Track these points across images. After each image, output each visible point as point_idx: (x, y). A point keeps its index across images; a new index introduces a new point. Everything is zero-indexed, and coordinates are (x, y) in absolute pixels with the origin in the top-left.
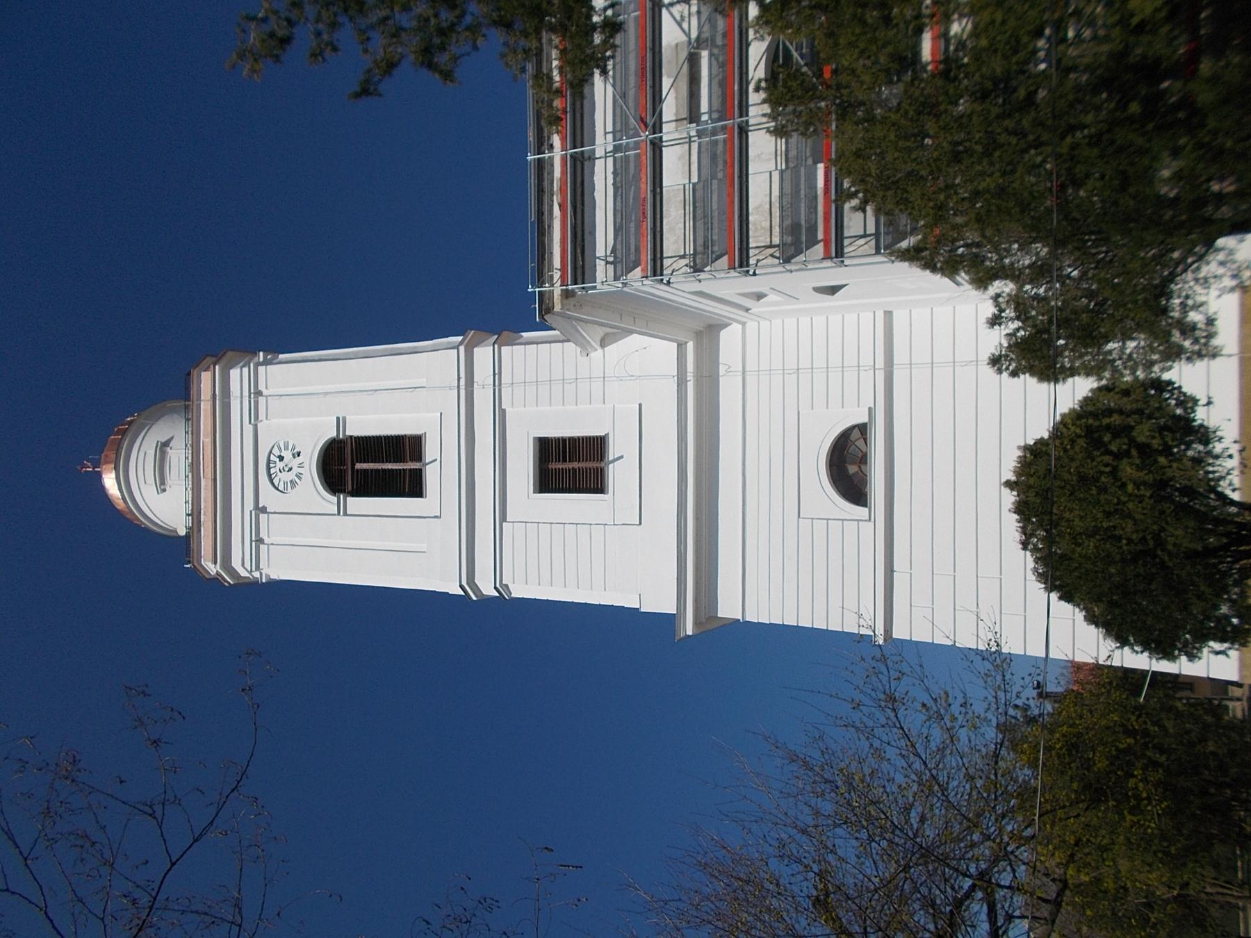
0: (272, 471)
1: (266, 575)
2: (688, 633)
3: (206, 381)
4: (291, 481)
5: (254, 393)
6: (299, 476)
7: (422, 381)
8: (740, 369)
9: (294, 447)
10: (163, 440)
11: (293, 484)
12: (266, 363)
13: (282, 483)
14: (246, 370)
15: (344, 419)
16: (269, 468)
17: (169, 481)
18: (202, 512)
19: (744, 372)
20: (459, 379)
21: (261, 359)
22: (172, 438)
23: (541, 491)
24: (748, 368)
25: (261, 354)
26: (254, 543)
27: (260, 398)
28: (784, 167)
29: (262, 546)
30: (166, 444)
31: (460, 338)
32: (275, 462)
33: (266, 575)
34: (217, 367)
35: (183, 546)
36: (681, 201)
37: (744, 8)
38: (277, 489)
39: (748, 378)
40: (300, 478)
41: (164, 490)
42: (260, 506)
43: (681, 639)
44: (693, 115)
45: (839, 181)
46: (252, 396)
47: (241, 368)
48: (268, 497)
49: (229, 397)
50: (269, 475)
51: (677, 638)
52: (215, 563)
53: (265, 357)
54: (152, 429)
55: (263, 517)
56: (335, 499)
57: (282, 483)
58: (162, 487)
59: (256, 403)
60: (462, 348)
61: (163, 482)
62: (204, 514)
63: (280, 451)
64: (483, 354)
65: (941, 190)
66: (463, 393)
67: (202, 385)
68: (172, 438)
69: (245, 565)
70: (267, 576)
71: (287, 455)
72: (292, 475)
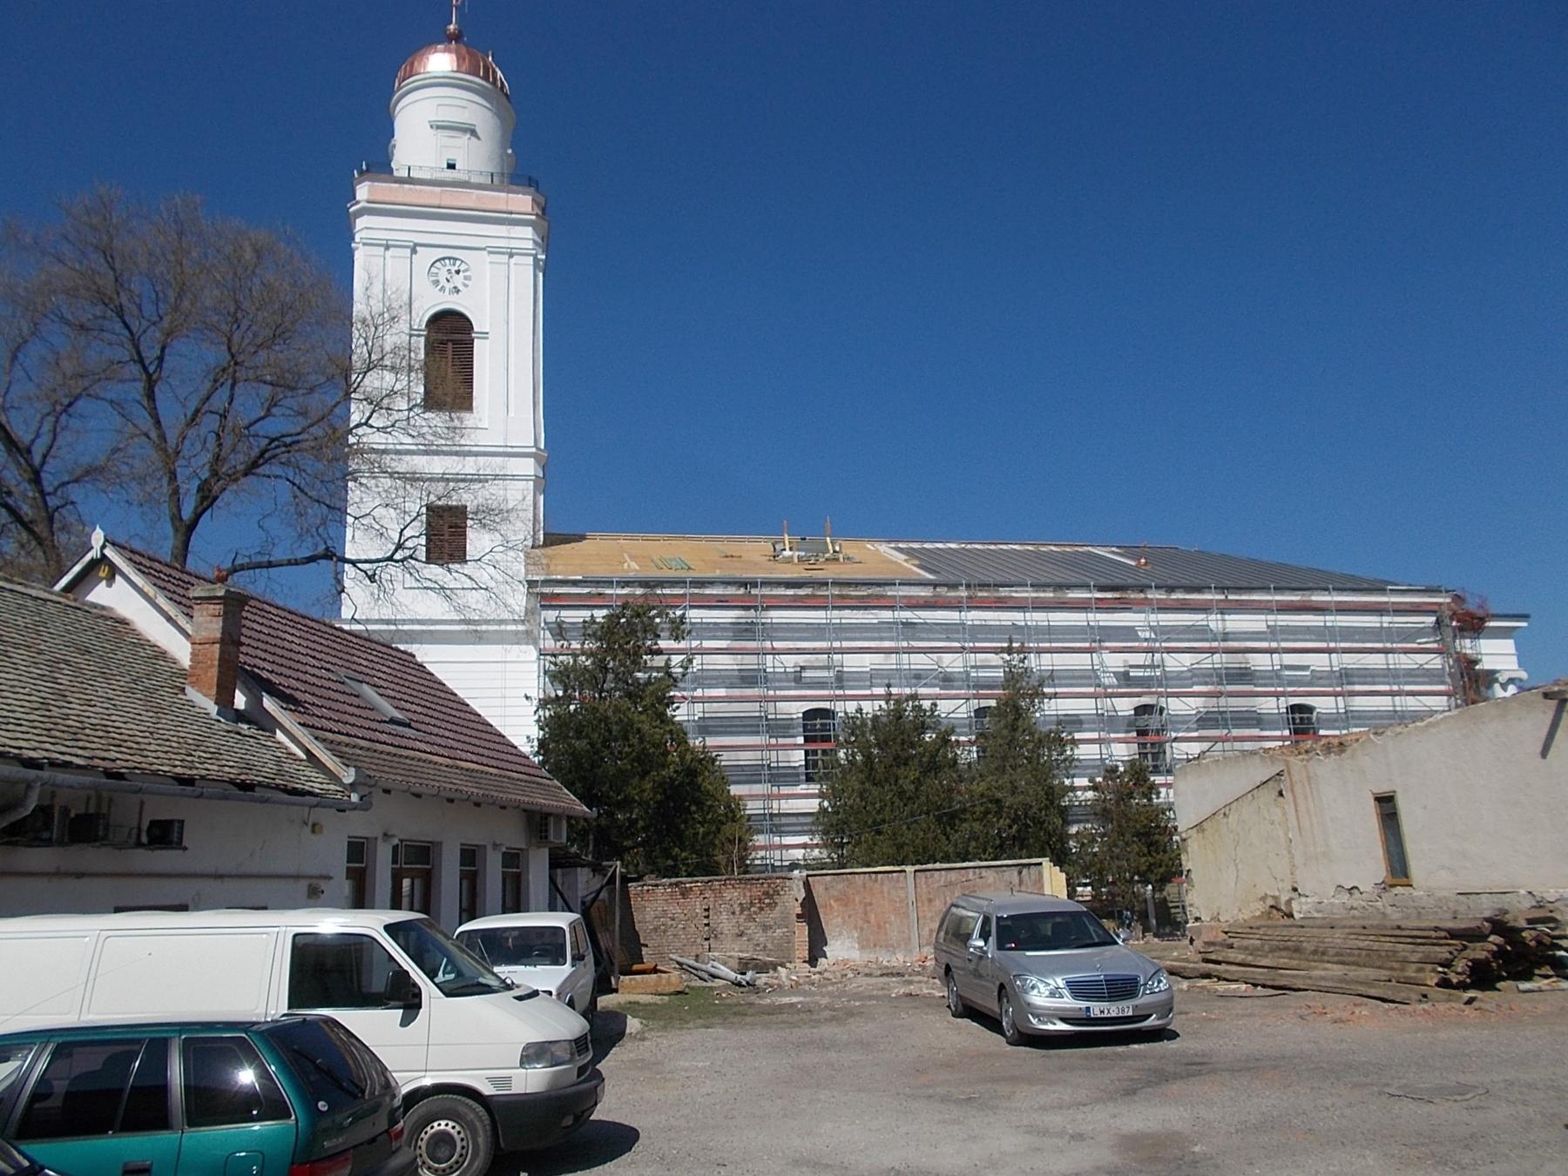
0: (447, 261)
3: (522, 202)
4: (438, 281)
7: (512, 414)
8: (508, 660)
9: (466, 286)
10: (477, 130)
11: (436, 282)
12: (536, 260)
13: (436, 271)
14: (530, 245)
15: (487, 338)
16: (449, 258)
18: (412, 186)
19: (505, 662)
20: (512, 447)
21: (539, 257)
22: (478, 138)
24: (507, 665)
29: (382, 249)
30: (473, 133)
31: (542, 447)
32: (454, 265)
34: (534, 217)
35: (381, 166)
36: (49, 431)
37: (1093, 726)
38: (432, 265)
39: (499, 665)
40: (440, 290)
41: (432, 127)
42: (418, 248)
43: (235, 684)
48: (426, 257)
49: (509, 224)
50: (444, 259)
51: (238, 683)
52: (368, 202)
53: (542, 260)
54: (486, 110)
55: (408, 251)
56: (423, 327)
57: (436, 271)
59: (503, 253)
60: (534, 450)
61: (438, 127)
62: (410, 189)
63: (465, 271)
64: (528, 467)
65: (783, 1152)
66: (501, 450)
67: (520, 196)
68: (478, 138)
69: (365, 231)
70: (357, 248)
71: (458, 280)
72: (443, 282)
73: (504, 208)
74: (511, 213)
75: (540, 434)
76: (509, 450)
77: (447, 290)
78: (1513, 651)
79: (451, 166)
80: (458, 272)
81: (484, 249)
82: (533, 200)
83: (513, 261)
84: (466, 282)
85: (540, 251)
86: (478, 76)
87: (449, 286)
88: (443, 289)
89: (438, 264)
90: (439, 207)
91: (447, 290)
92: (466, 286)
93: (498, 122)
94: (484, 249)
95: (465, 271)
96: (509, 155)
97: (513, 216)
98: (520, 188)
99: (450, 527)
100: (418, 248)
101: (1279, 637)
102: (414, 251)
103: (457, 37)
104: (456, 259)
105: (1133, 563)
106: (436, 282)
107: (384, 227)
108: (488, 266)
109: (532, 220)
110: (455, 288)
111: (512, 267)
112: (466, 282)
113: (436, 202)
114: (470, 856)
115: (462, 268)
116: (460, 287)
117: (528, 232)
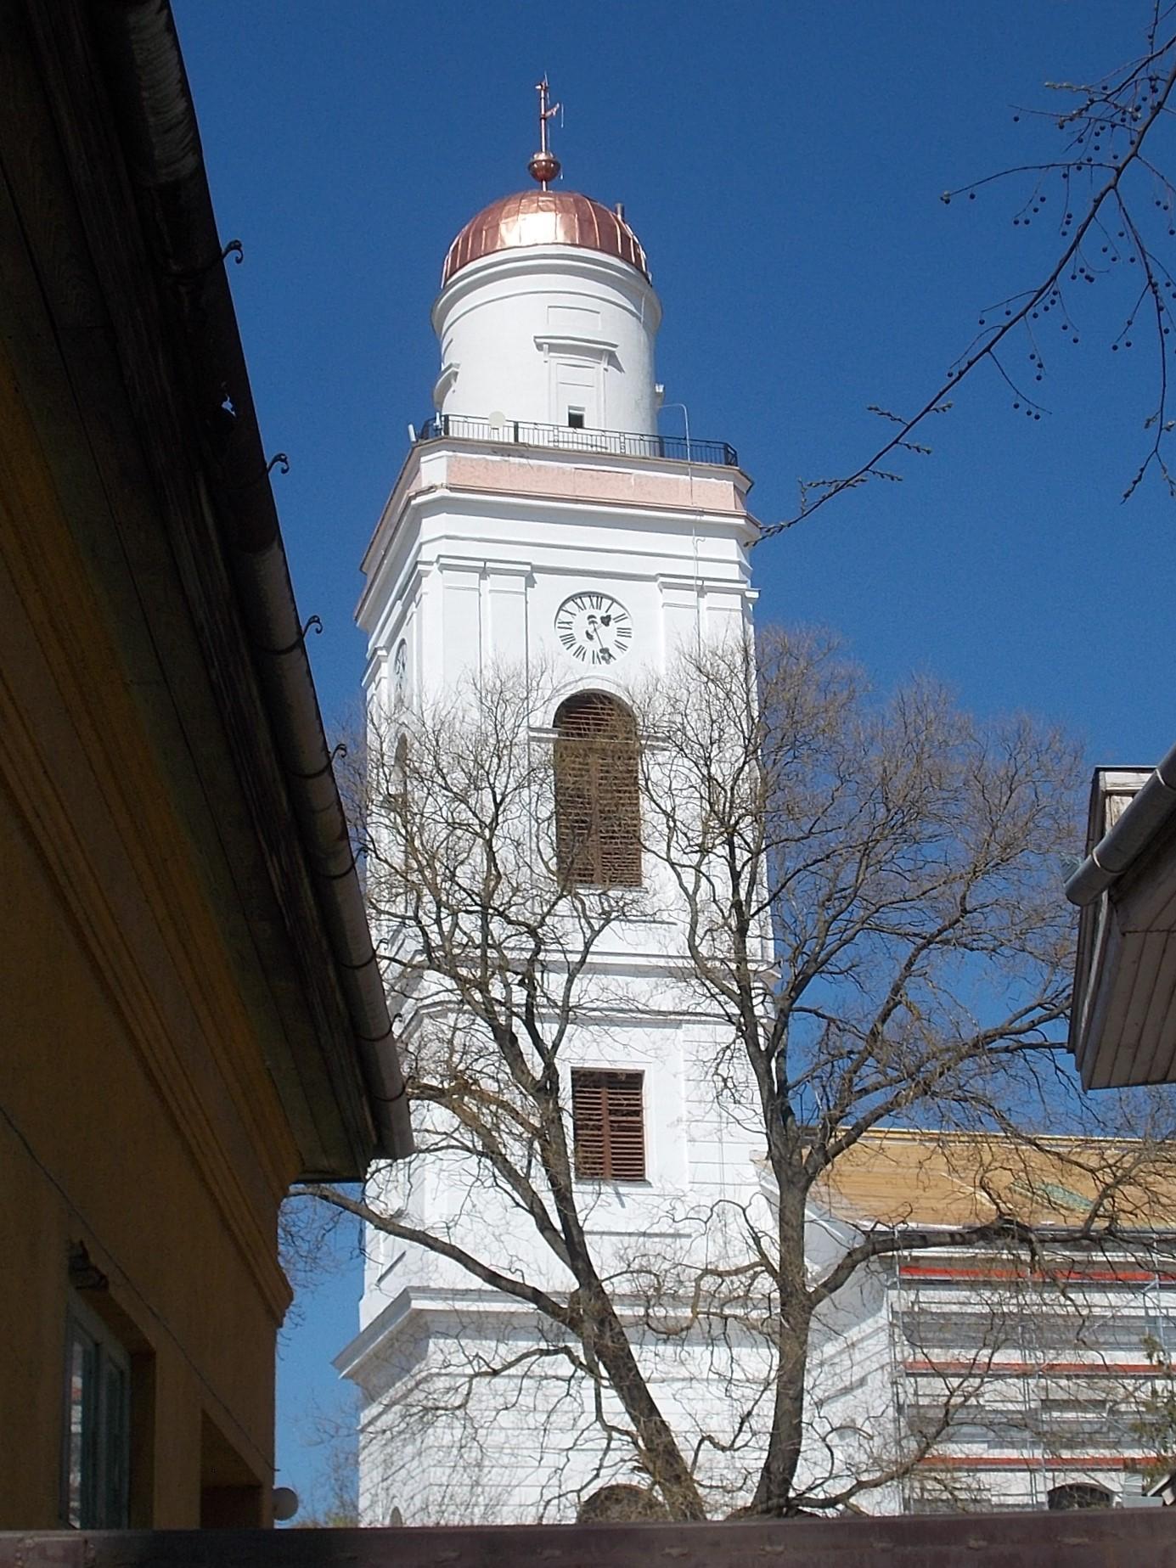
0: (586, 600)
1: (429, 572)
2: (413, 1302)
5: (702, 587)
6: (581, 652)
9: (622, 647)
10: (618, 352)
11: (568, 640)
13: (568, 618)
14: (734, 572)
16: (590, 594)
17: (557, 359)
18: (524, 461)
22: (620, 370)
23: (573, 1073)
25: (755, 595)
26: (481, 564)
27: (696, 593)
28: (987, 1408)
30: (612, 359)
33: (429, 572)
34: (742, 522)
41: (539, 347)
44: (1048, 1404)
45: (398, 1230)
46: (700, 583)
47: (739, 563)
48: (552, 589)
50: (580, 595)
52: (451, 489)
57: (568, 618)
58: (546, 346)
59: (689, 588)
61: (553, 348)
62: (520, 465)
63: (621, 618)
67: (713, 480)
68: (620, 370)
70: (428, 573)
71: (608, 636)
72: (581, 639)
73: (687, 503)
74: (703, 513)
77: (589, 655)
78: (587, 1239)
79: (576, 421)
80: (606, 621)
81: (653, 579)
82: (735, 486)
83: (706, 601)
84: (620, 639)
86: (616, 255)
87: (592, 647)
88: (581, 652)
89: (568, 606)
90: (577, 501)
91: (589, 655)
92: (622, 647)
94: (653, 579)
95: (621, 618)
96: (658, 394)
97: (706, 518)
98: (714, 467)
99: (611, 1112)
100: (535, 575)
101: (454, 1319)
102: (530, 582)
103: (547, 176)
104: (601, 596)
105: (413, 439)
106: (568, 640)
107: (477, 536)
109: (738, 526)
110: (604, 650)
111: (704, 614)
112: (620, 639)
113: (568, 491)
115: (615, 611)
116: (613, 650)
117: (730, 549)
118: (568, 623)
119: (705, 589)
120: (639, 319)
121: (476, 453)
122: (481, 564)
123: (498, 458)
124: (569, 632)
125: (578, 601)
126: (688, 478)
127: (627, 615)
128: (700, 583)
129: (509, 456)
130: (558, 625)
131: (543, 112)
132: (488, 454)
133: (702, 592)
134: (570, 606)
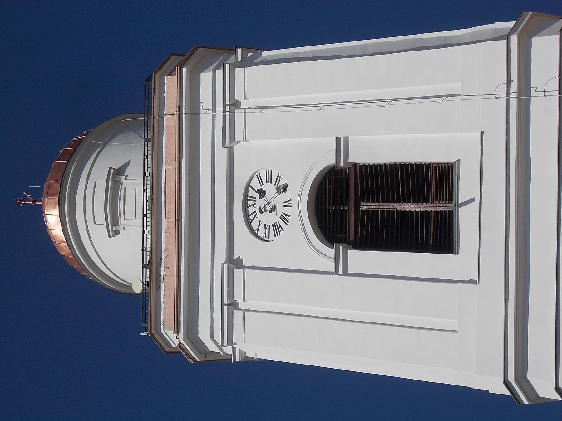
4: (275, 225)
7: (456, 87)
9: (279, 178)
11: (277, 228)
13: (262, 228)
15: (346, 140)
17: (123, 222)
22: (128, 164)
26: (226, 308)
31: (511, 24)
34: (184, 69)
38: (256, 235)
41: (117, 233)
46: (227, 107)
47: (214, 70)
55: (238, 273)
56: (331, 252)
57: (262, 228)
60: (514, 39)
61: (115, 223)
63: (261, 183)
67: (165, 95)
68: (128, 164)
70: (242, 353)
74: (180, 107)
75: (495, 30)
76: (514, 87)
82: (169, 75)
85: (232, 59)
89: (255, 228)
93: (121, 136)
97: (184, 104)
104: (246, 198)
106: (277, 228)
108: (253, 143)
109: (190, 73)
114: (269, 183)
118: (266, 229)
119: (233, 102)
120: (105, 145)
121: (161, 303)
122: (226, 308)
123: (162, 285)
124: (271, 227)
125: (251, 217)
126: (165, 117)
127: (257, 174)
128: (227, 107)
129: (161, 276)
130: (267, 239)
131: (31, 203)
132: (161, 293)
133: (235, 105)
134: (255, 225)
